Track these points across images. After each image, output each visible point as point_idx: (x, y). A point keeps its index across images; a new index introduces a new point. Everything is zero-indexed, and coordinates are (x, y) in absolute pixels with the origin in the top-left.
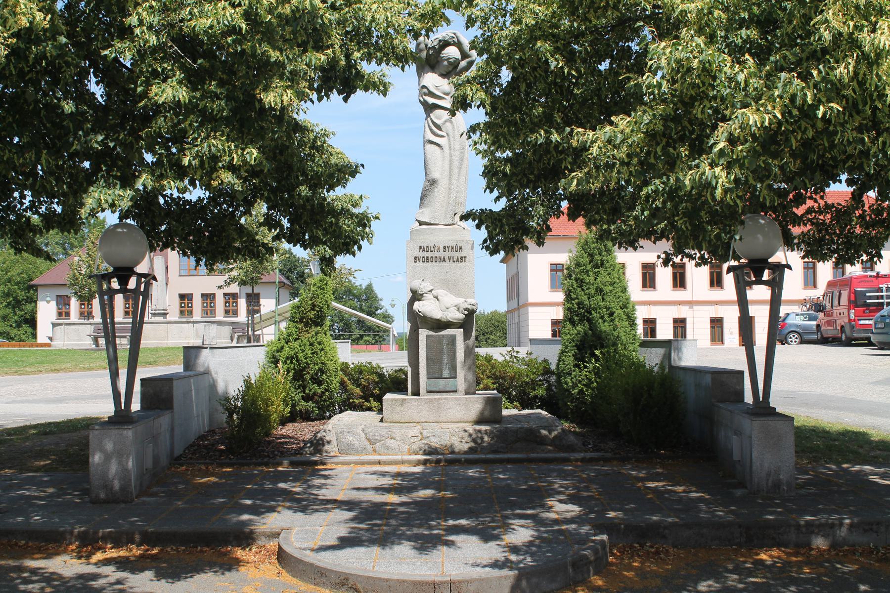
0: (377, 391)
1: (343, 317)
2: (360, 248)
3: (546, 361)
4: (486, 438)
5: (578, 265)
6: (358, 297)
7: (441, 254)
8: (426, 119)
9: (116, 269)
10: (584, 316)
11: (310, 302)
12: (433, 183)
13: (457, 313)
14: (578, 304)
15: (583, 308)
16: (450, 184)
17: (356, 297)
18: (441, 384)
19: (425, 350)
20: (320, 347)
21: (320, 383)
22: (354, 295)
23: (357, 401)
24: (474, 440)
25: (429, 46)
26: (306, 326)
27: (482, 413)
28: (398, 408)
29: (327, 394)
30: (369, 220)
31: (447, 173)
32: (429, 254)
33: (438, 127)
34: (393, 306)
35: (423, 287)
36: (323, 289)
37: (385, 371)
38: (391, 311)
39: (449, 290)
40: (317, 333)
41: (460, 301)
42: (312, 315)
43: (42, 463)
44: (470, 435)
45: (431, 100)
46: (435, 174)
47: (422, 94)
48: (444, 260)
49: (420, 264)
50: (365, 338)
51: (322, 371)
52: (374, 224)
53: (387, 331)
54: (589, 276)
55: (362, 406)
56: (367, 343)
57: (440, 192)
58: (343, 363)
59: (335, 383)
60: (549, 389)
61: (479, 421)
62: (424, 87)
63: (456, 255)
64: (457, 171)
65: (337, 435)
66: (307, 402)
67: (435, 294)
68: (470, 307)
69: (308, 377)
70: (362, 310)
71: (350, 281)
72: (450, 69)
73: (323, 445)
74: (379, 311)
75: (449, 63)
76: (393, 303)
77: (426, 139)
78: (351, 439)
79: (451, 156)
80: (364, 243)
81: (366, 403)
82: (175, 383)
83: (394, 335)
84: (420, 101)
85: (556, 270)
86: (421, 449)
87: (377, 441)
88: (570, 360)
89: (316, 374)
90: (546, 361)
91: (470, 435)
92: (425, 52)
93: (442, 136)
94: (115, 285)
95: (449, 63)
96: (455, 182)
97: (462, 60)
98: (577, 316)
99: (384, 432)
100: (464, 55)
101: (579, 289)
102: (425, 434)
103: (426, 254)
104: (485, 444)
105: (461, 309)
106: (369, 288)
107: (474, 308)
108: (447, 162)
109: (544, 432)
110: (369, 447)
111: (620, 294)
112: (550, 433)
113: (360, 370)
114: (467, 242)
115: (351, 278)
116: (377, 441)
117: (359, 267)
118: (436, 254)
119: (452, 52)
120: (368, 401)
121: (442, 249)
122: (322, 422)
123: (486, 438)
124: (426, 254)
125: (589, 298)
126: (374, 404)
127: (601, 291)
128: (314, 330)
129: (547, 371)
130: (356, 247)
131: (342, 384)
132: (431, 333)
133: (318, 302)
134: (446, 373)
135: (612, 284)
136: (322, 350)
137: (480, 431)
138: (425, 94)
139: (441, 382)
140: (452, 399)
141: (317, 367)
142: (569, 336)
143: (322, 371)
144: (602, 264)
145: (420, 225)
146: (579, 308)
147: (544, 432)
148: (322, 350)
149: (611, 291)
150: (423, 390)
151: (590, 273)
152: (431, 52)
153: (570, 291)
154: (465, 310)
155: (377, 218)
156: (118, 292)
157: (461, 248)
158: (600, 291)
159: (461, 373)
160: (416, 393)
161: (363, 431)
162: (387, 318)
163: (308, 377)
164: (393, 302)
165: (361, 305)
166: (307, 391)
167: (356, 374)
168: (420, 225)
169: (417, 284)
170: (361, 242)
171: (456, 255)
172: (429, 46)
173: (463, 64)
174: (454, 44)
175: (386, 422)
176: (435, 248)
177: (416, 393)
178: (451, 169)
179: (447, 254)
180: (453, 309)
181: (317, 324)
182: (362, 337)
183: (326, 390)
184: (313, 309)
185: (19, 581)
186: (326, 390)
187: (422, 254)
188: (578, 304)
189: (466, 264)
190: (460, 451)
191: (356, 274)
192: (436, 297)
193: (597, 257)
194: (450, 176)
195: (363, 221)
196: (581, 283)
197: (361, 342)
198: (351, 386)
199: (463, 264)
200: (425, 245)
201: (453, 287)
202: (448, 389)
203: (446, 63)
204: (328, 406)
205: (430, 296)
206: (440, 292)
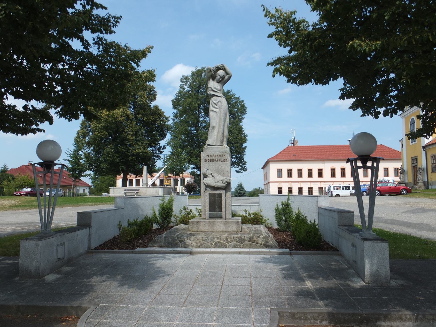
7: (216, 158)
9: (359, 156)
32: (211, 158)
41: (222, 178)
43: (11, 262)
48: (217, 161)
68: (228, 181)
82: (93, 215)
93: (217, 108)
94: (359, 164)
100: (227, 74)
107: (230, 181)
118: (214, 158)
119: (221, 72)
124: (209, 158)
134: (217, 210)
156: (360, 167)
171: (223, 158)
173: (227, 77)
179: (219, 158)
185: (427, 313)
187: (208, 158)
199: (225, 163)
200: (209, 154)
206: (215, 174)
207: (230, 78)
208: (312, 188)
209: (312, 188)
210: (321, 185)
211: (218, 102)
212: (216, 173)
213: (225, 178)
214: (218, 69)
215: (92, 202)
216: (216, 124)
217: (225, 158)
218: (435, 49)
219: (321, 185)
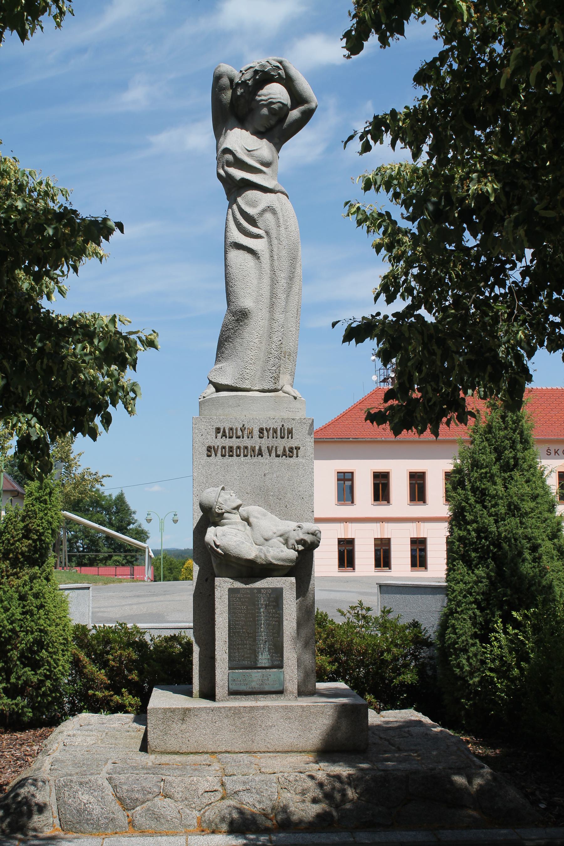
0: (134, 676)
1: (89, 532)
2: (107, 421)
3: (415, 625)
4: (351, 793)
5: (476, 465)
6: (107, 510)
7: (255, 442)
8: (230, 207)
10: (488, 551)
11: (21, 525)
12: (240, 317)
13: (284, 548)
14: (478, 531)
15: (486, 538)
16: (272, 319)
17: (105, 509)
18: (255, 677)
19: (226, 615)
20: (38, 602)
21: (35, 665)
22: (102, 506)
23: (99, 694)
24: (328, 796)
25: (237, 80)
26: (13, 566)
27: (333, 730)
28: (177, 727)
29: (48, 683)
30: (131, 348)
31: (266, 299)
32: (234, 442)
33: (252, 220)
34: (149, 521)
35: (225, 500)
36: (45, 502)
37: (147, 638)
38: (145, 527)
39: (270, 508)
40: (33, 578)
41: (289, 526)
42: (24, 546)
44: (321, 785)
45: (238, 174)
46: (246, 301)
47: (221, 163)
48: (260, 454)
49: (217, 460)
50: (115, 558)
51: (40, 644)
52: (143, 355)
53: (141, 551)
54: (495, 483)
55: (108, 703)
56: (117, 564)
57: (254, 333)
58: (77, 627)
59: (63, 663)
60: (421, 671)
61: (327, 752)
62: (227, 151)
63: (282, 444)
64: (283, 296)
65: (59, 789)
66: (14, 698)
67: (245, 514)
69: (15, 654)
70: (111, 525)
71: (98, 490)
72: (272, 122)
73: (30, 815)
74: (131, 526)
75: (271, 111)
76: (149, 517)
77: (230, 240)
78: (85, 798)
79: (273, 271)
80: (117, 412)
81: (117, 698)
83: (150, 557)
84: (219, 176)
85: (344, 480)
86: (223, 819)
87: (136, 802)
88: (465, 627)
89: (30, 650)
90: (415, 625)
91: (321, 785)
92: (229, 93)
93: (258, 236)
95: (271, 111)
96: (279, 316)
97: (293, 107)
98: (476, 550)
99: (150, 782)
100: (298, 98)
101: (478, 506)
102: (230, 786)
103: (227, 442)
104: (348, 806)
105: (292, 541)
106: (121, 499)
108: (266, 281)
109: (460, 780)
110: (121, 816)
111: (546, 515)
112: (470, 782)
113: (106, 638)
114: (301, 422)
115: (98, 486)
116: (136, 802)
117: (99, 457)
118: (247, 442)
119: (276, 92)
120: (119, 693)
121: (256, 433)
122: (40, 732)
123: (351, 793)
124: (227, 442)
125: (496, 522)
126: (129, 699)
127: (517, 508)
128: (26, 572)
129: (420, 641)
130: (98, 420)
131: (76, 663)
132: (238, 585)
133: (34, 524)
134: (264, 659)
135: (534, 498)
136: (41, 606)
137: (338, 777)
138: (229, 164)
139: (256, 674)
140: (277, 709)
141: (30, 638)
142: (462, 585)
143: (40, 644)
144: (516, 465)
145: (218, 390)
146: (479, 538)
147: (460, 780)
148: (41, 606)
149: (533, 510)
150: (221, 688)
151: (498, 480)
152: (239, 92)
153: (463, 509)
154: (299, 542)
155: (151, 344)
157: (290, 432)
158: (513, 509)
159: (290, 654)
160: (209, 694)
161: (110, 780)
162: (141, 535)
163: (15, 654)
164: (168, 531)
165: (110, 519)
166: (13, 680)
167: (97, 645)
168: (218, 390)
169: (211, 495)
170: (110, 409)
171: (282, 444)
172: (237, 80)
173: (295, 114)
174: (280, 80)
175: (154, 752)
176: (245, 431)
177: (209, 694)
178: (273, 295)
179: (265, 443)
180: (277, 542)
181: (33, 563)
182: (110, 557)
183: (47, 677)
184: (26, 537)
186: (47, 677)
187: (220, 442)
188: (478, 531)
189: (300, 460)
190: (301, 821)
191: (104, 481)
192: (246, 520)
193: (509, 454)
194: (272, 306)
195: (118, 351)
196: (482, 495)
197: (109, 562)
198: (91, 668)
199: (293, 460)
201: (279, 501)
202: (267, 688)
203: (265, 111)
204: (51, 703)
205: (235, 518)
206: (254, 510)
207: (307, 115)
208: (351, 542)
209: (351, 542)
210: (346, 530)
211: (264, 211)
212: (255, 503)
213: (294, 525)
214: (263, 77)
215: (304, 680)
216: (257, 301)
217: (293, 443)
218: (23, 2)
219: (346, 530)
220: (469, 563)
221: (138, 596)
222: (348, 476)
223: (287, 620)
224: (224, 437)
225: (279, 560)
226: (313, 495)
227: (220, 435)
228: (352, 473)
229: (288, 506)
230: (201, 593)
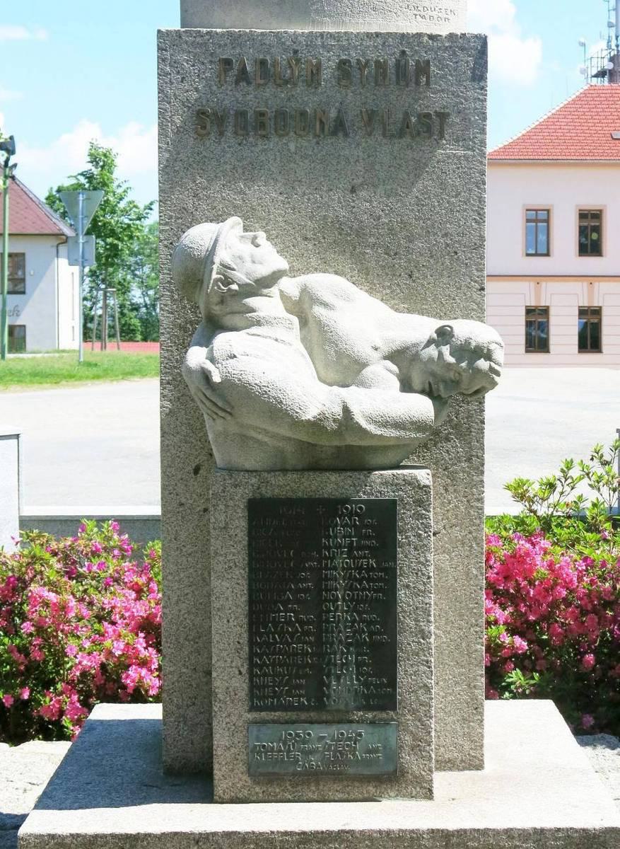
48: (340, 127)
118: (308, 100)
179: (353, 100)
180: (384, 375)
187: (230, 97)
220: (345, 361)
221: (520, 159)
222: (542, 215)
223: (408, 587)
224: (243, 84)
225: (385, 424)
226: (482, 246)
227: (231, 77)
228: (548, 211)
229: (416, 274)
230: (182, 504)
